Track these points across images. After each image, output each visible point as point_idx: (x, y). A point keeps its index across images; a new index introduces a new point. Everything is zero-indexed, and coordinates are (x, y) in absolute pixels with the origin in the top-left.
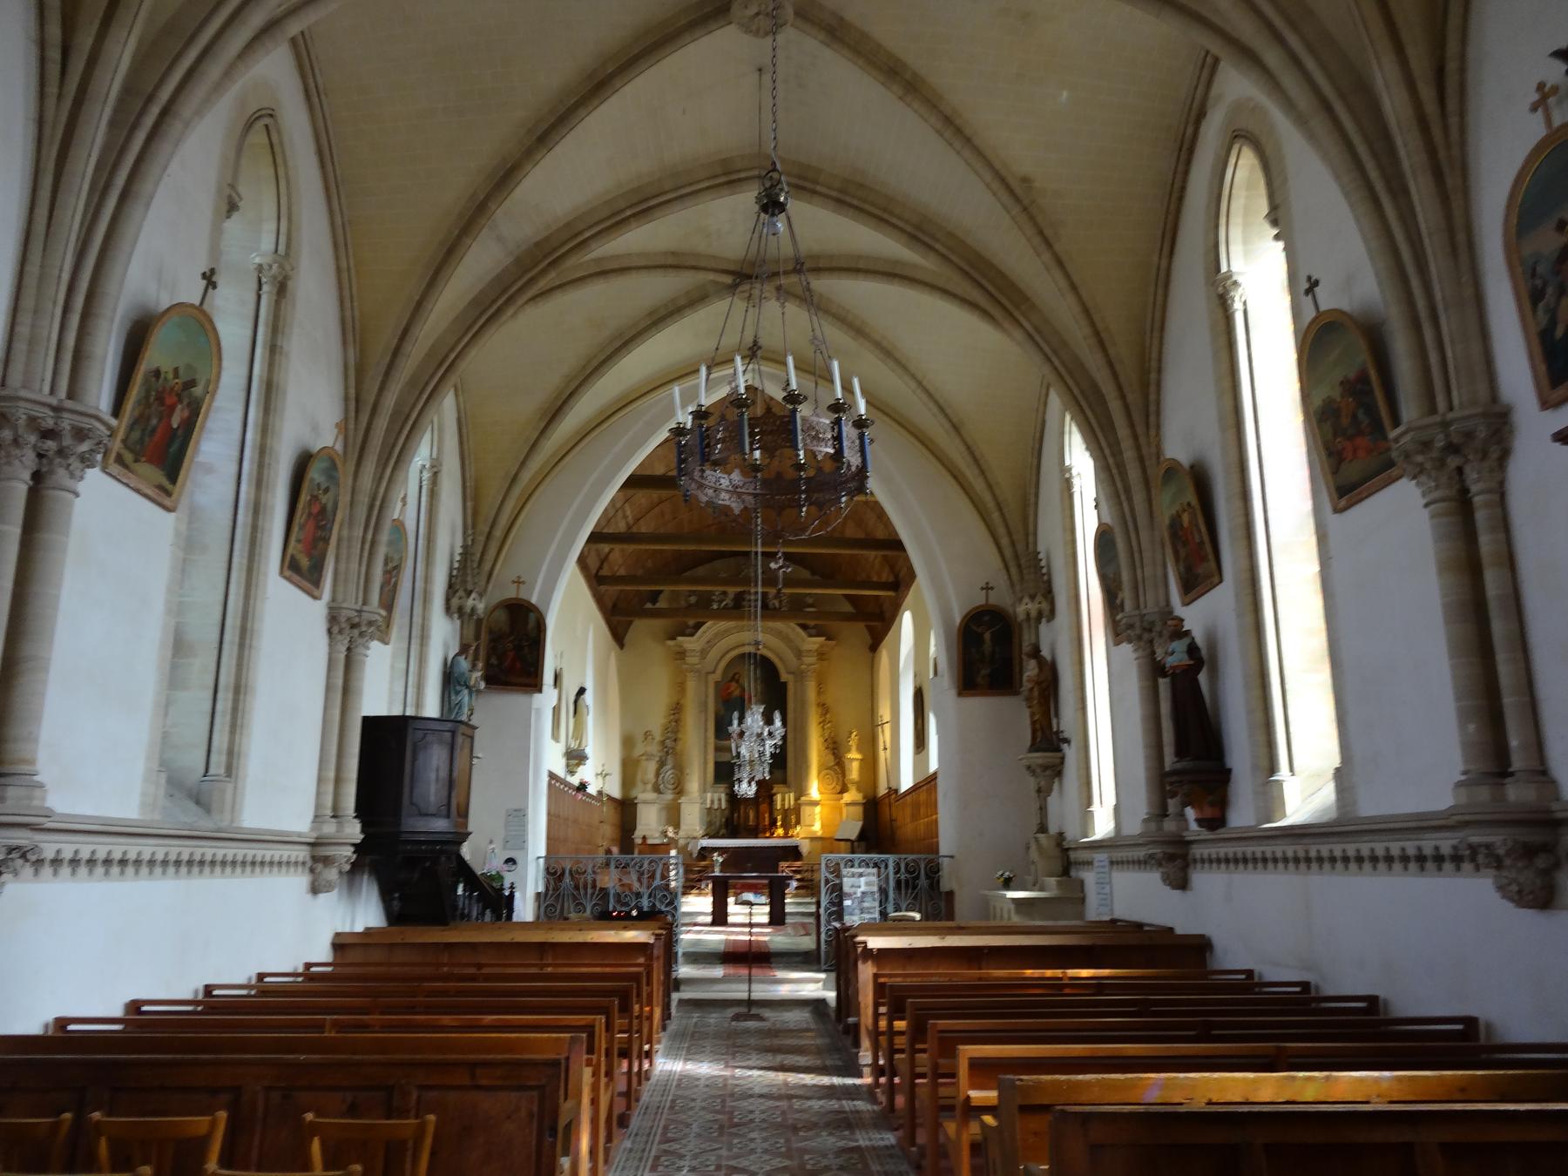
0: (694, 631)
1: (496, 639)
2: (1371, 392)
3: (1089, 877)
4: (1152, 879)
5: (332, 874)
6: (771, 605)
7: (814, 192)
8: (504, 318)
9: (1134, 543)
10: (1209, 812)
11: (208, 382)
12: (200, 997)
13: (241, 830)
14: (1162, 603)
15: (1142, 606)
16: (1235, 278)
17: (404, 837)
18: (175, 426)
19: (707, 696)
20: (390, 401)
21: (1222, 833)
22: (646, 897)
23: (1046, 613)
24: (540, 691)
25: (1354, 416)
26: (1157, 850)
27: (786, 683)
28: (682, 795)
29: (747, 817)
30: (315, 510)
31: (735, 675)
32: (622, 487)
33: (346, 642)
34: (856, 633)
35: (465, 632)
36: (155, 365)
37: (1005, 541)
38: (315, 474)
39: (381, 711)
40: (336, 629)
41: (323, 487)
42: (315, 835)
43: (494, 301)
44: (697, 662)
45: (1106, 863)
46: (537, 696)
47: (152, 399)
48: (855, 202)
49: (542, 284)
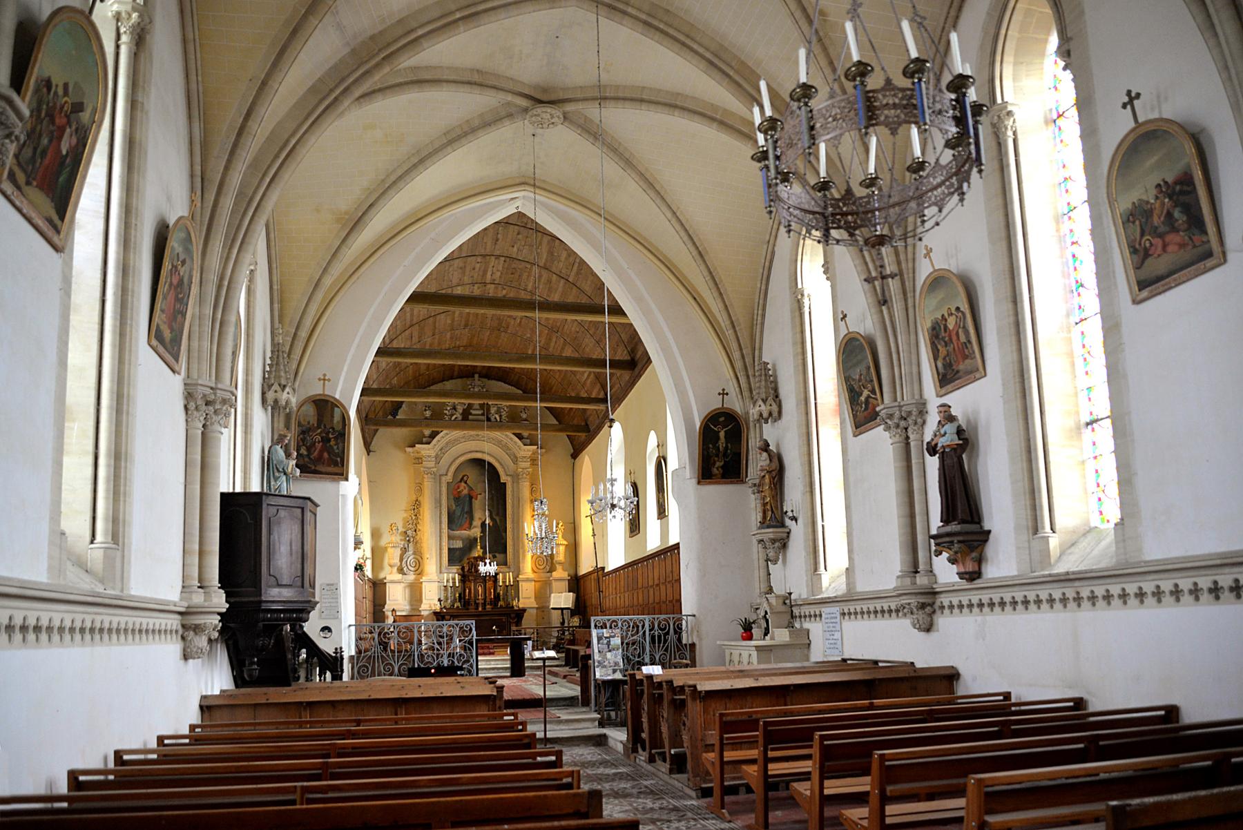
0: (429, 440)
1: (304, 432)
2: (1194, 191)
3: (816, 629)
4: (903, 625)
5: (202, 642)
6: (493, 419)
7: (625, 13)
8: (341, 108)
9: (893, 345)
10: (970, 566)
11: (95, 110)
12: (111, 765)
13: (132, 598)
16: (1010, 108)
17: (264, 606)
18: (64, 152)
19: (440, 494)
20: (235, 179)
21: (978, 583)
22: (445, 657)
23: (775, 414)
24: (347, 479)
25: (1169, 215)
27: (505, 483)
28: (423, 575)
29: (476, 591)
30: (175, 281)
31: (464, 476)
32: (408, 301)
33: (202, 418)
34: (561, 440)
35: (276, 425)
36: (46, 74)
37: (736, 355)
38: (174, 245)
39: (225, 490)
40: (192, 406)
41: (181, 258)
42: (186, 604)
43: (332, 91)
44: (433, 465)
45: (838, 615)
46: (343, 483)
47: (43, 115)
48: (661, 26)
49: (375, 80)
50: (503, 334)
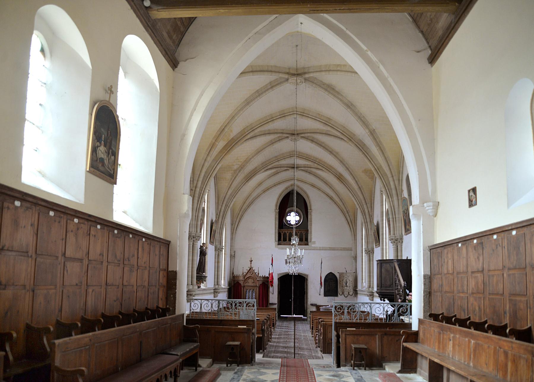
14: (372, 247)
15: (395, 234)
26: (368, 294)
50: (225, 306)
